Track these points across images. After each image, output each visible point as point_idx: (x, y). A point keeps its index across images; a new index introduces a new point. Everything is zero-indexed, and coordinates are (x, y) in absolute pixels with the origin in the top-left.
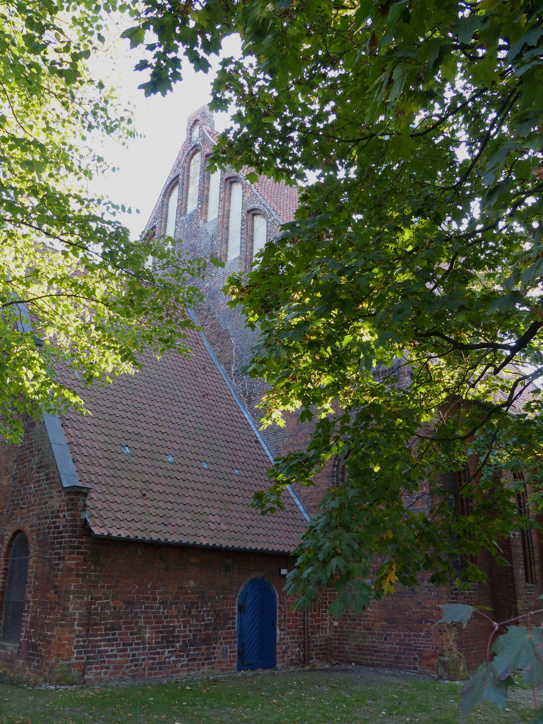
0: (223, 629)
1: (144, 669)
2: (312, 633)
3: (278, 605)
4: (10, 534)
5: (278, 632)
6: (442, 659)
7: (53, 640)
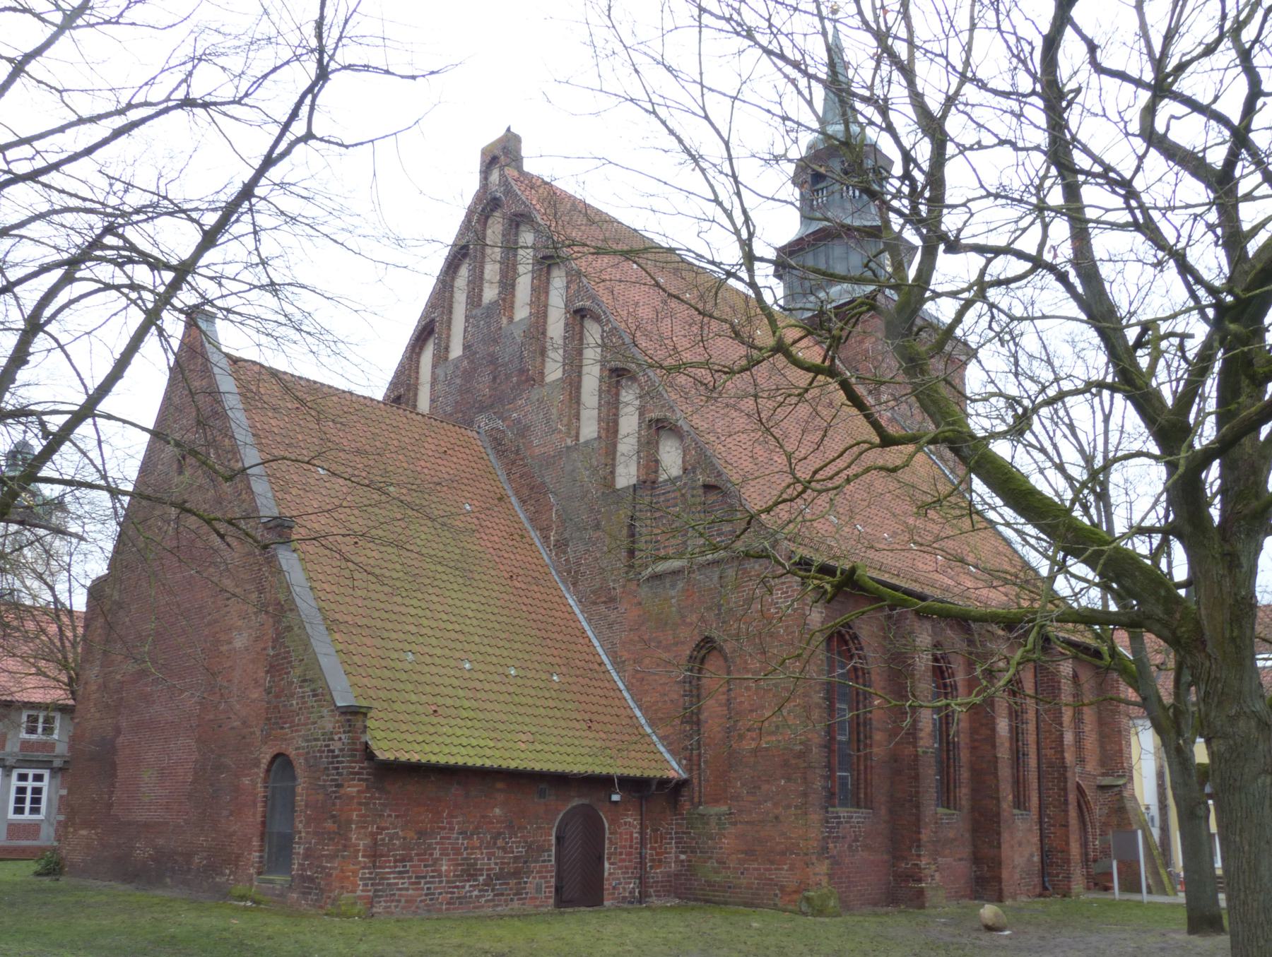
0: (536, 861)
1: (441, 904)
2: (651, 867)
3: (607, 835)
4: (269, 757)
5: (607, 865)
6: (807, 894)
7: (334, 873)
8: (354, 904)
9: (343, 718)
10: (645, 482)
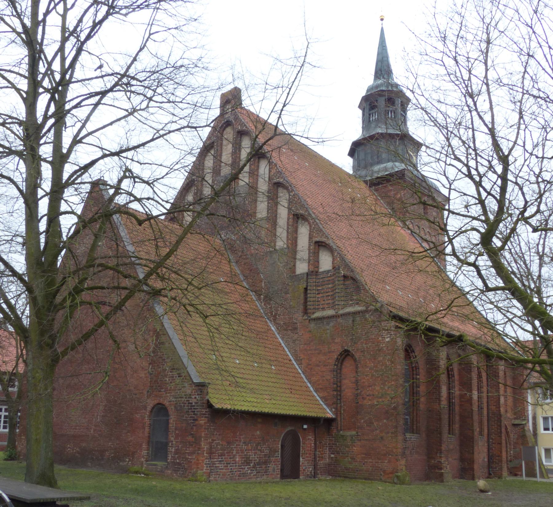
0: (273, 457)
1: (236, 476)
2: (319, 460)
3: (301, 445)
4: (152, 405)
5: (301, 459)
6: (397, 474)
8: (203, 475)
9: (197, 388)
10: (312, 272)
